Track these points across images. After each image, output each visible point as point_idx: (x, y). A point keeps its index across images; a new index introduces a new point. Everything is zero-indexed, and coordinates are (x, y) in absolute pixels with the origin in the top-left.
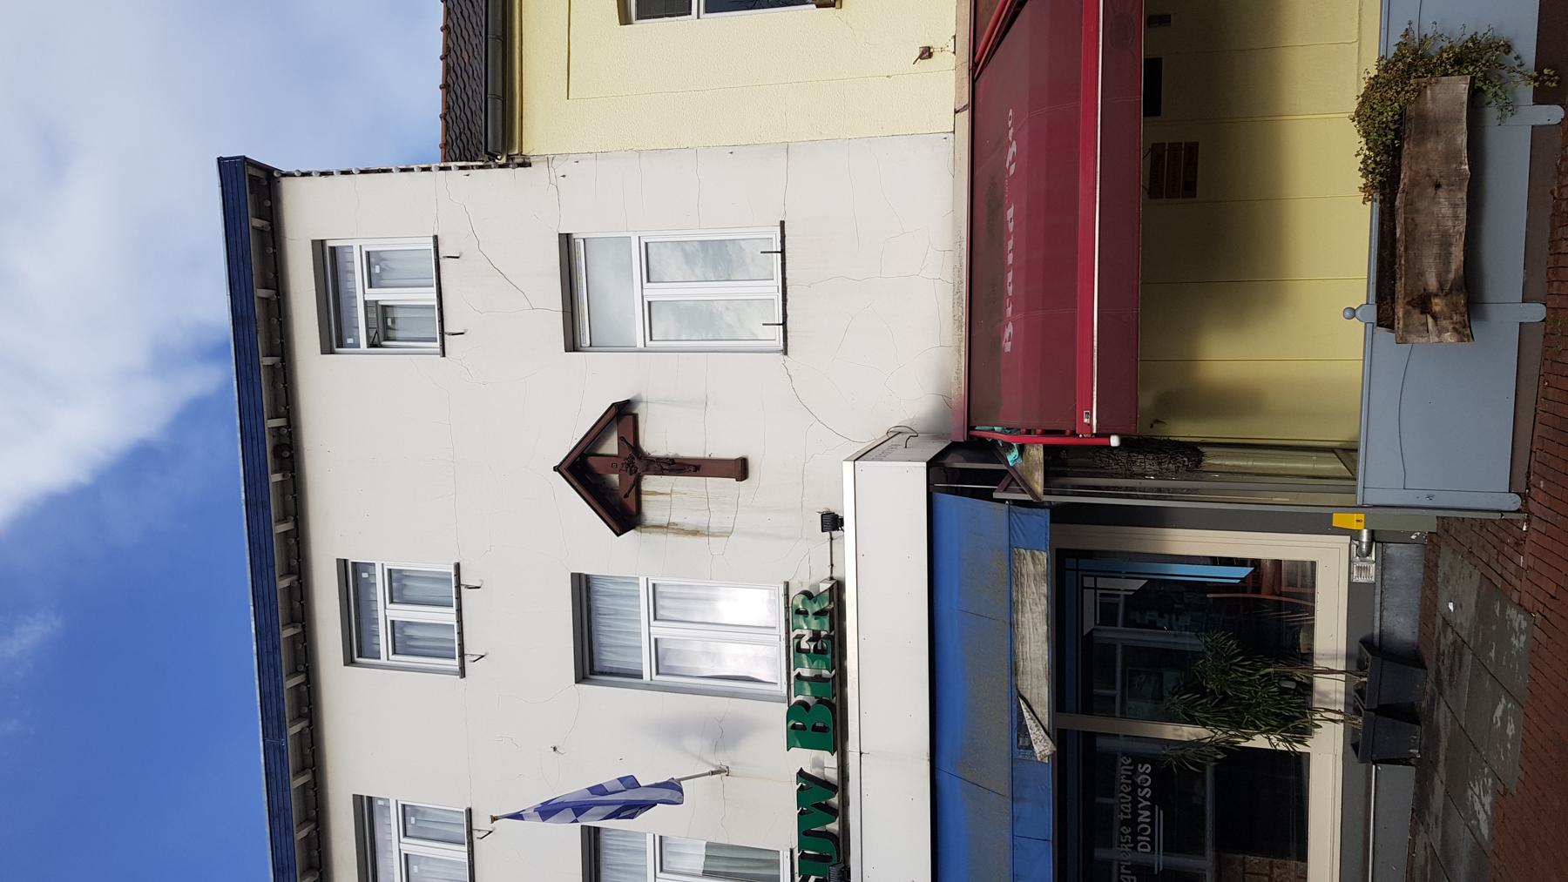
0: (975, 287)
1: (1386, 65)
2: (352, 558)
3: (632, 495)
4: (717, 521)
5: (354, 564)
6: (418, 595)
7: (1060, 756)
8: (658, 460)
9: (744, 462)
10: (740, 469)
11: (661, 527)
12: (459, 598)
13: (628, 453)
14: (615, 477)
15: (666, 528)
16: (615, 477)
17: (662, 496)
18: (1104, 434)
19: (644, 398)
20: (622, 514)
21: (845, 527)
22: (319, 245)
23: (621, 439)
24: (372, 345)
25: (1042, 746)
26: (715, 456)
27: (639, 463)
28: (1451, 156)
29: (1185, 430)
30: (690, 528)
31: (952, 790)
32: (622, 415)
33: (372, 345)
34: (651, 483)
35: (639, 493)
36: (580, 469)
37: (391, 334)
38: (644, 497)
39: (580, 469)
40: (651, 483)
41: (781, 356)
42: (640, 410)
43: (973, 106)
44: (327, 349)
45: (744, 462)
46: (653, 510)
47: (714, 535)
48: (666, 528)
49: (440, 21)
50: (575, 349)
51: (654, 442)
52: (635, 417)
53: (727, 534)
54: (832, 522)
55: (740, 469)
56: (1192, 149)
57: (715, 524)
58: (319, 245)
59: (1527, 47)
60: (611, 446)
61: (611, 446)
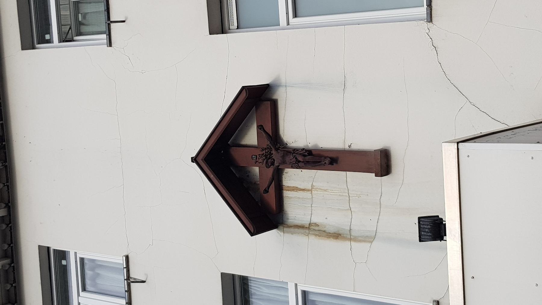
2: (55, 246)
3: (272, 190)
4: (360, 222)
5: (54, 250)
6: (89, 290)
8: (295, 151)
11: (302, 227)
12: (129, 291)
13: (266, 143)
14: (256, 169)
15: (308, 229)
16: (256, 169)
17: (305, 192)
19: (283, 81)
20: (260, 211)
21: (448, 237)
23: (260, 128)
24: (61, 40)
26: (355, 147)
27: (281, 155)
30: (332, 230)
32: (257, 102)
33: (61, 40)
34: (293, 177)
35: (279, 189)
36: (219, 159)
37: (84, 29)
38: (286, 194)
39: (219, 159)
40: (293, 177)
41: (425, 24)
42: (280, 95)
44: (28, 44)
46: (295, 209)
47: (356, 239)
48: (308, 229)
50: (223, 31)
51: (298, 129)
52: (274, 104)
53: (369, 239)
54: (433, 229)
60: (251, 137)
61: (251, 137)
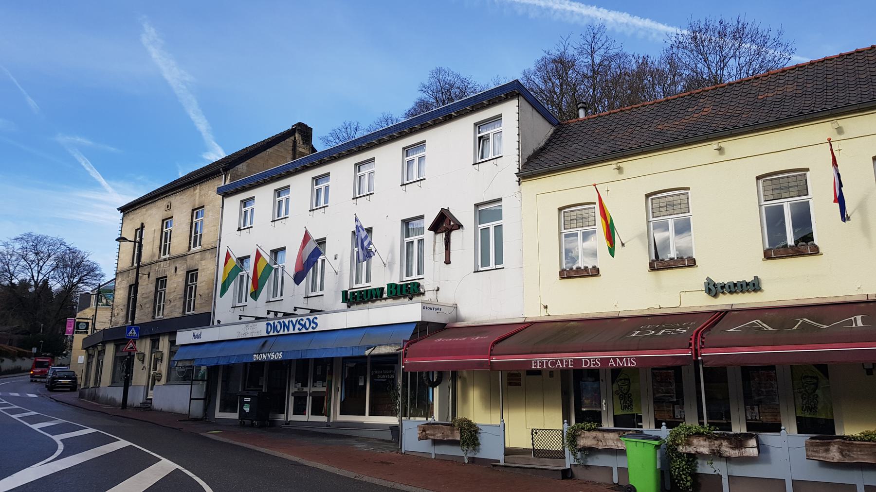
0: (346, 332)
1: (475, 425)
7: (365, 357)
9: (449, 263)
10: (448, 262)
17: (441, 237)
18: (404, 364)
20: (436, 227)
22: (501, 116)
25: (367, 353)
28: (448, 436)
29: (459, 384)
31: (396, 328)
32: (459, 226)
39: (406, 222)
43: (868, 302)
45: (449, 263)
49: (860, 47)
55: (448, 262)
56: (519, 384)
57: (436, 256)
58: (501, 116)
59: (478, 456)
